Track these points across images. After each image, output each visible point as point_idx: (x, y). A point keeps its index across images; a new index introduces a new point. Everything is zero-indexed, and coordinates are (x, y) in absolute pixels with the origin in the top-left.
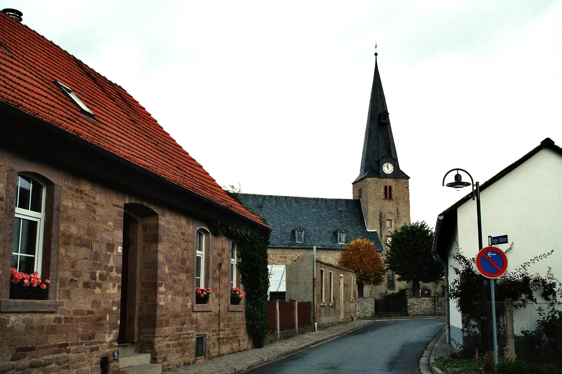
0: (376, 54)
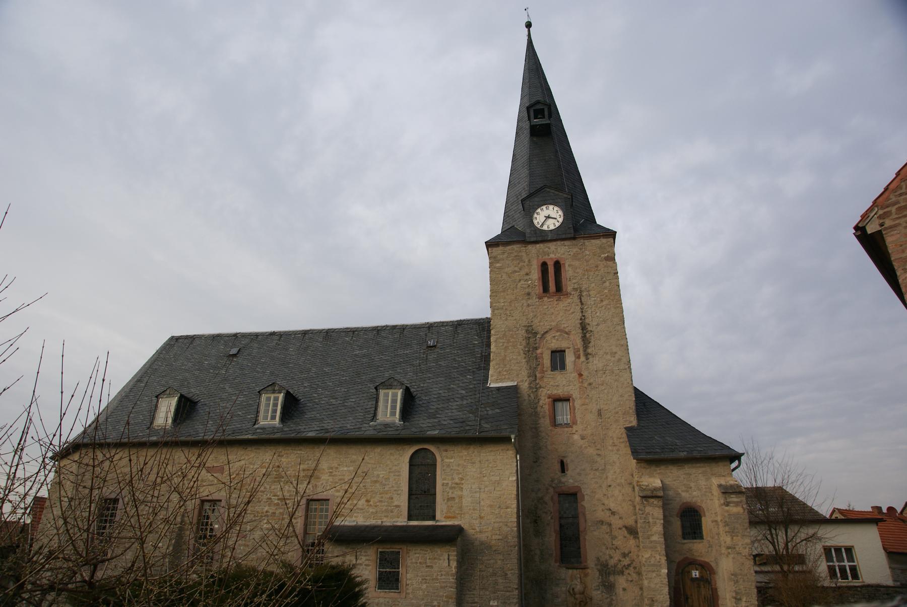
0: (529, 25)
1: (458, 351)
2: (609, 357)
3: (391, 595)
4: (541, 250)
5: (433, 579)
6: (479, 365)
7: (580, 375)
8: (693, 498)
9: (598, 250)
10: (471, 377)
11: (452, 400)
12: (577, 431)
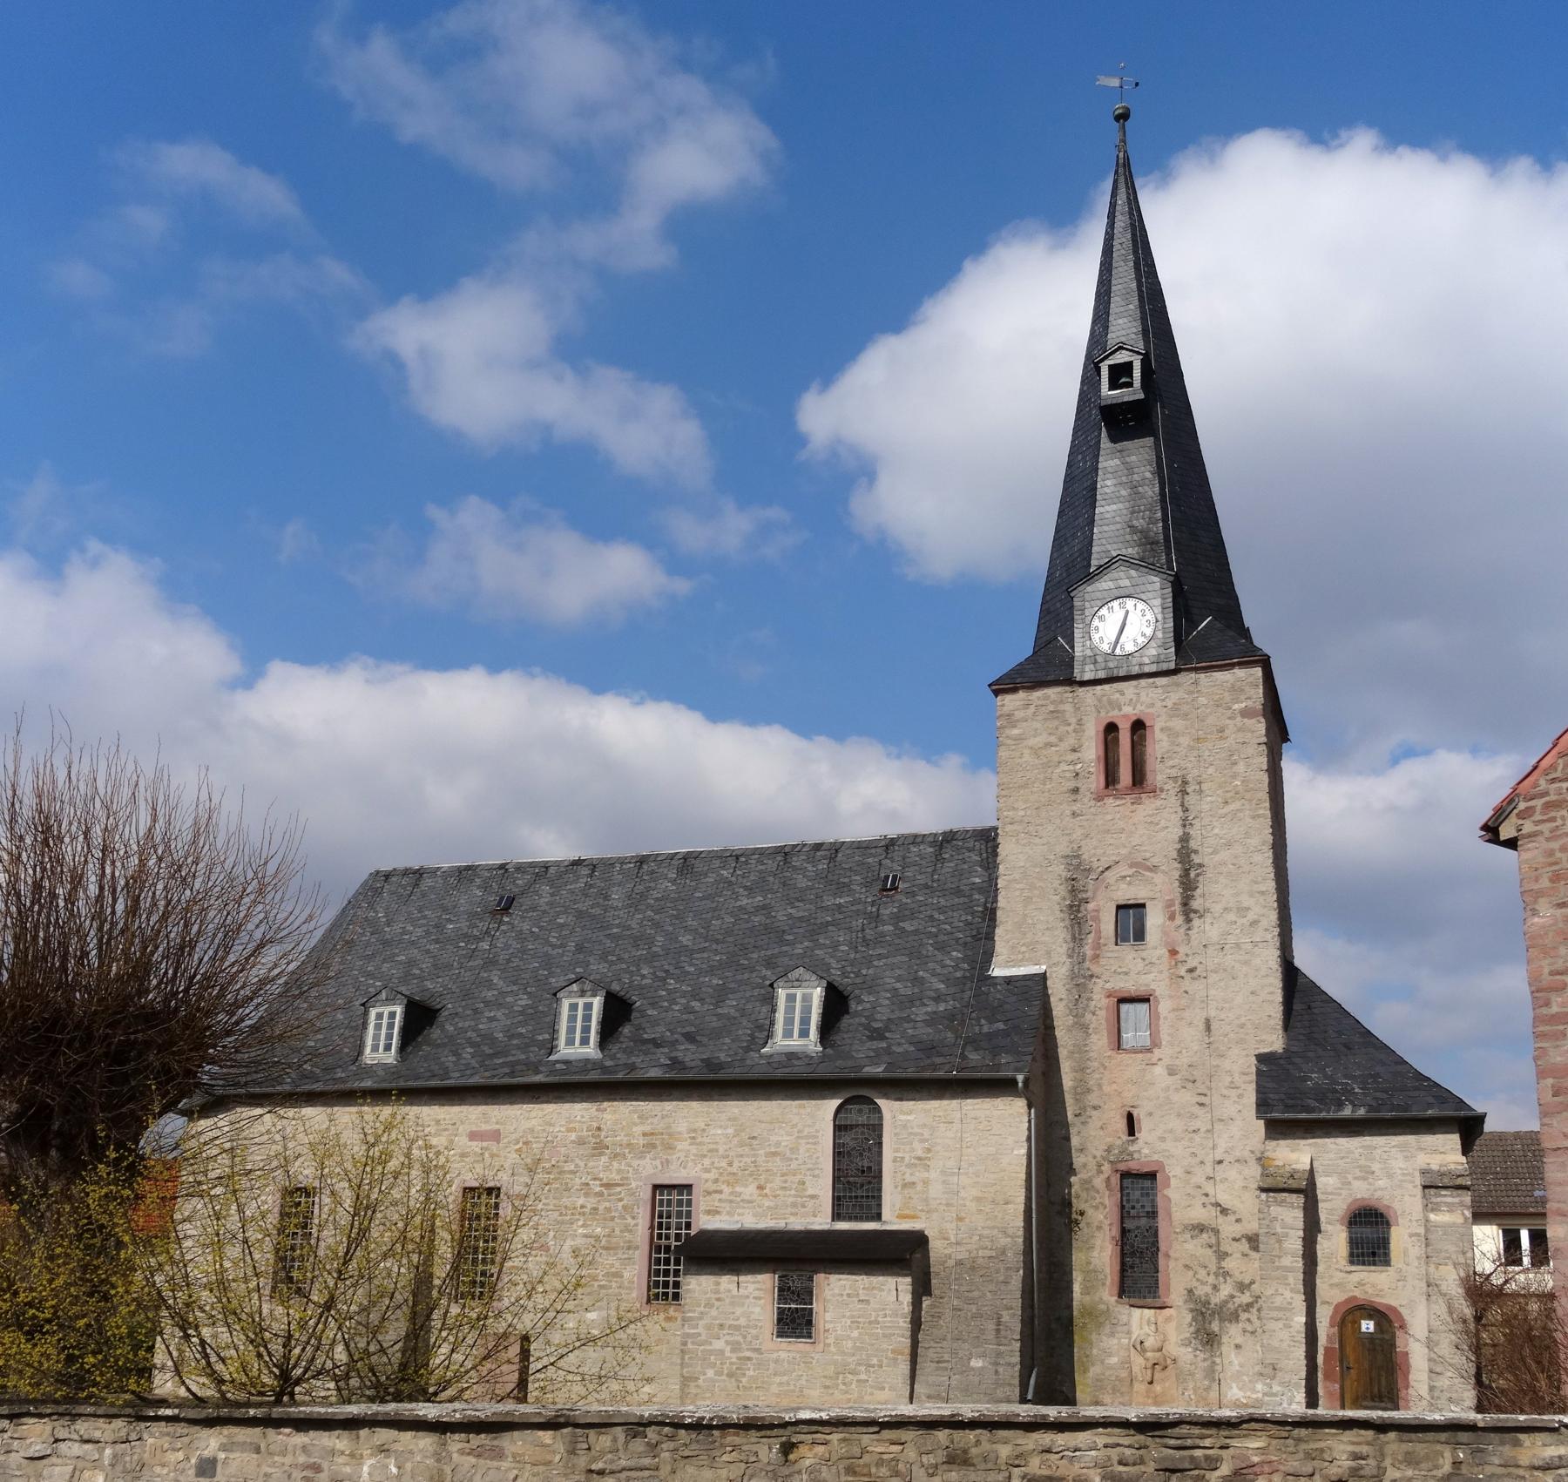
1: (941, 900)
2: (1231, 917)
3: (797, 1346)
4: (1105, 698)
5: (870, 1323)
6: (978, 929)
7: (1173, 952)
8: (1375, 1191)
9: (1226, 694)
10: (960, 955)
11: (918, 1003)
12: (1160, 1059)
